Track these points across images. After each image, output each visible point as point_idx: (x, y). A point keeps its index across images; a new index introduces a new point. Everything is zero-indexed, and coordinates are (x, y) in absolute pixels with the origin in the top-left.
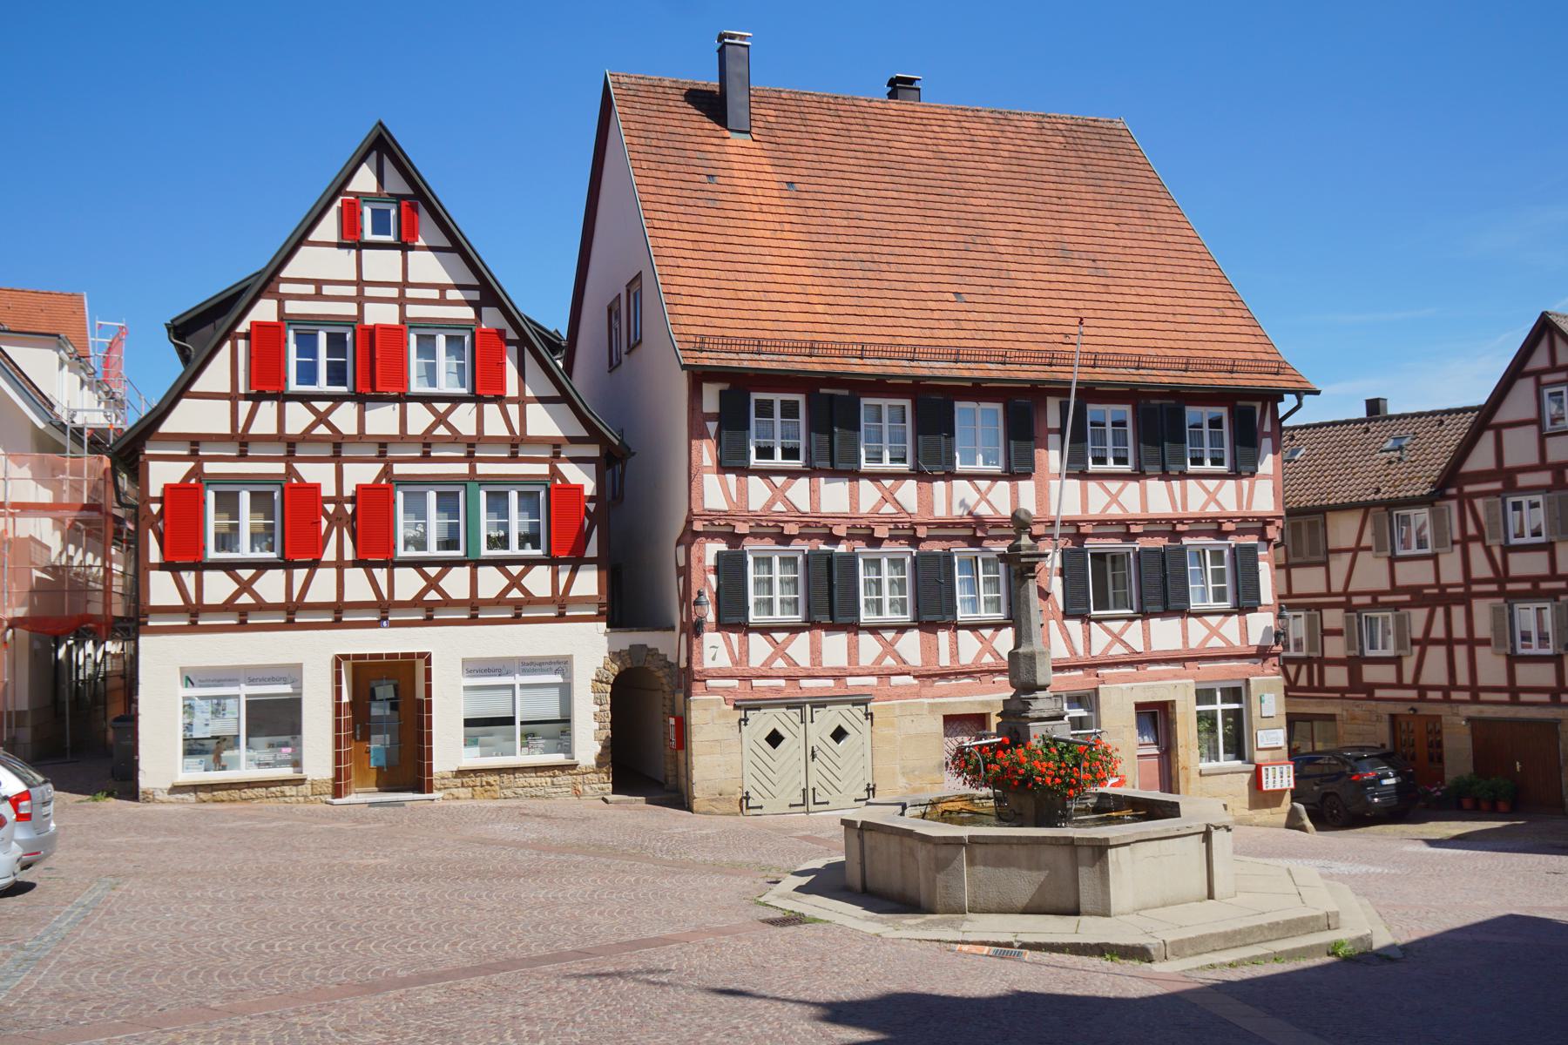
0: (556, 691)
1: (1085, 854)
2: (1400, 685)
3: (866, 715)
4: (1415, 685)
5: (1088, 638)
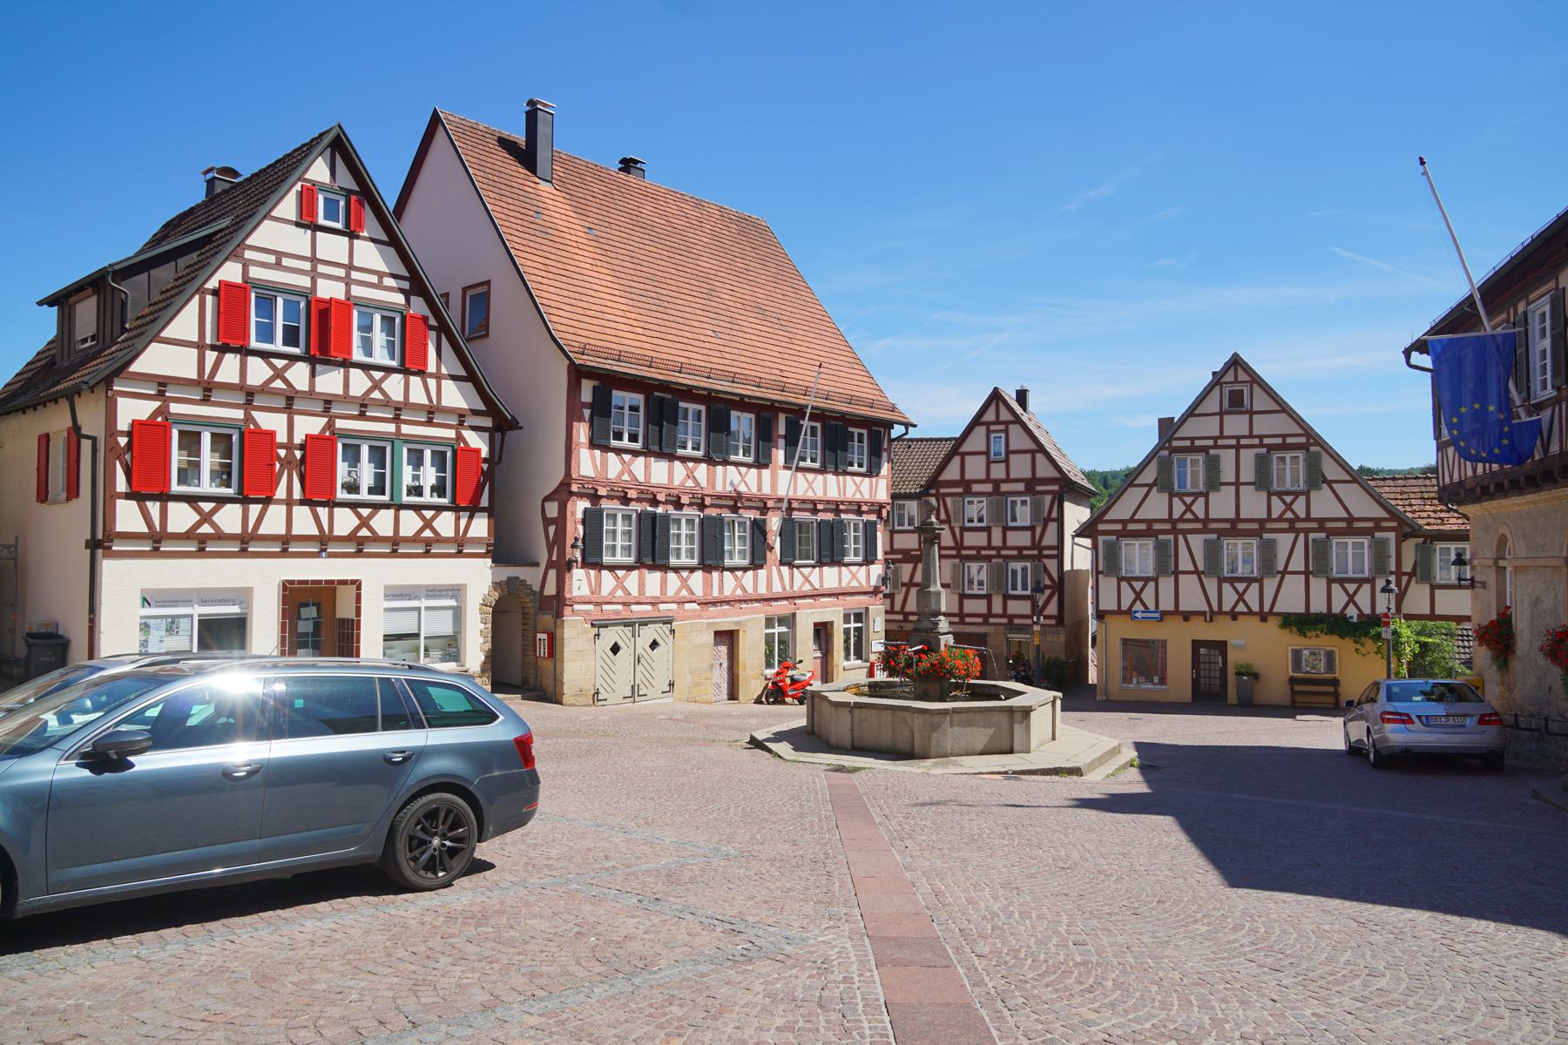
0: (451, 612)
1: (1018, 716)
4: (902, 612)
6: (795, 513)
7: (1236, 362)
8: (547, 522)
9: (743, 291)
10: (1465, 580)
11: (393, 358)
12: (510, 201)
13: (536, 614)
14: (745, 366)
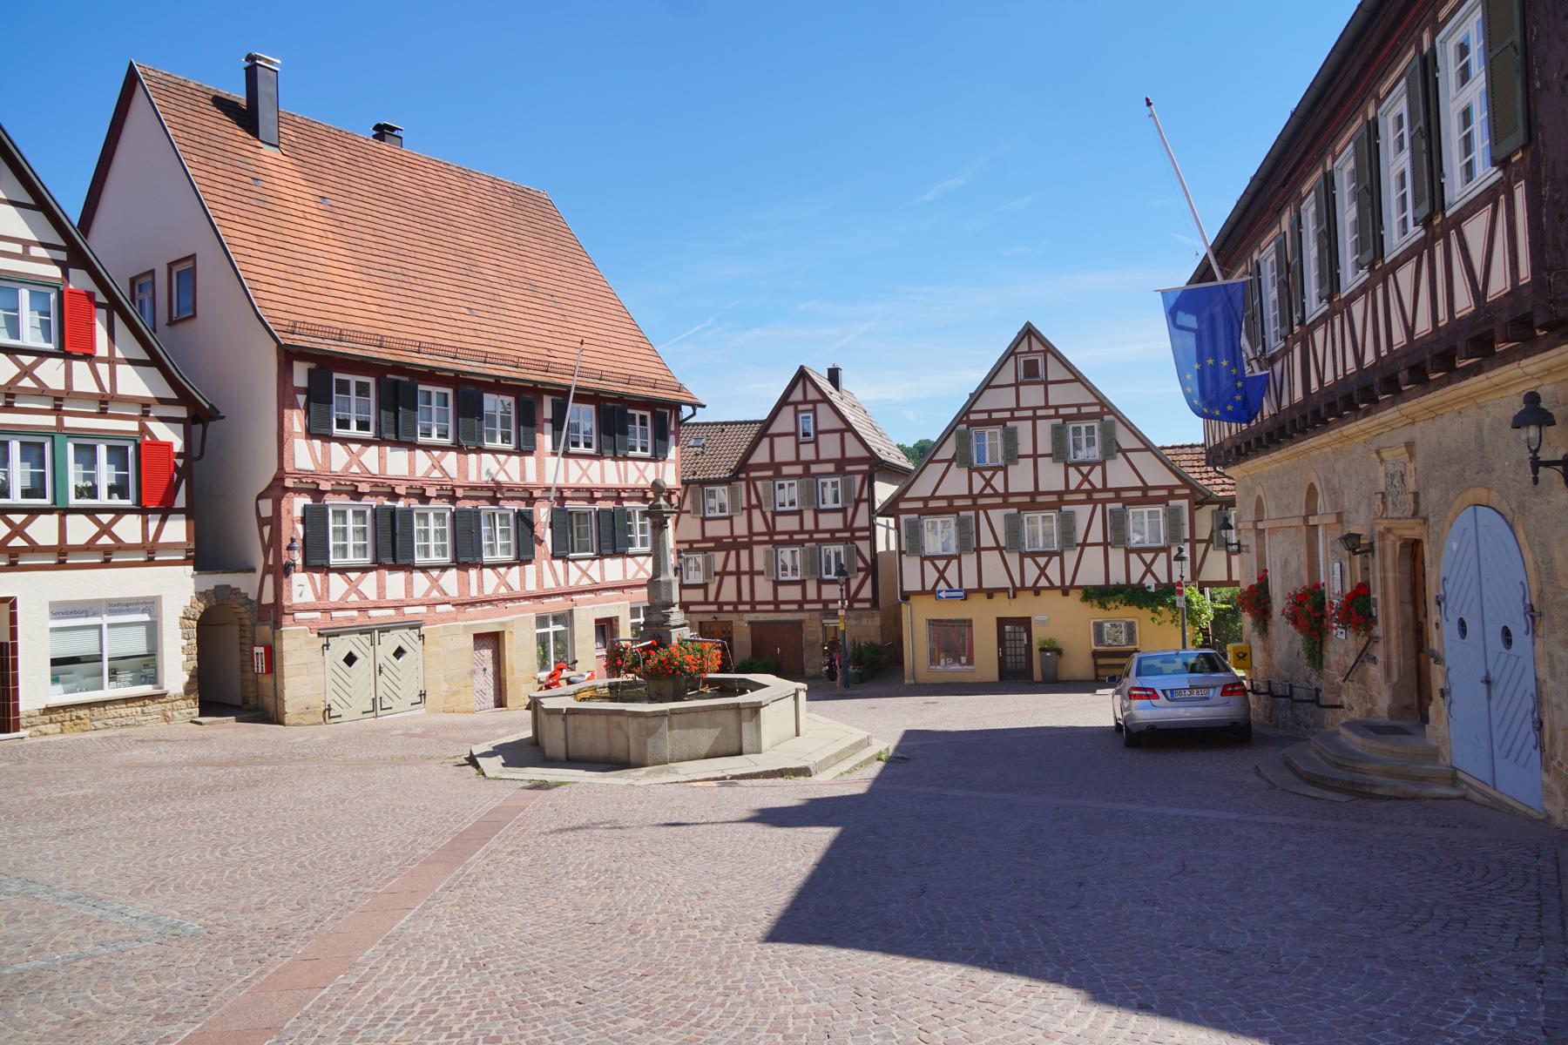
0: (143, 629)
1: (745, 713)
2: (706, 602)
3: (419, 636)
4: (716, 602)
5: (567, 573)
6: (568, 502)
7: (1029, 332)
8: (262, 522)
9: (511, 266)
10: (1232, 544)
11: (48, 340)
12: (219, 165)
13: (254, 625)
14: (505, 345)
